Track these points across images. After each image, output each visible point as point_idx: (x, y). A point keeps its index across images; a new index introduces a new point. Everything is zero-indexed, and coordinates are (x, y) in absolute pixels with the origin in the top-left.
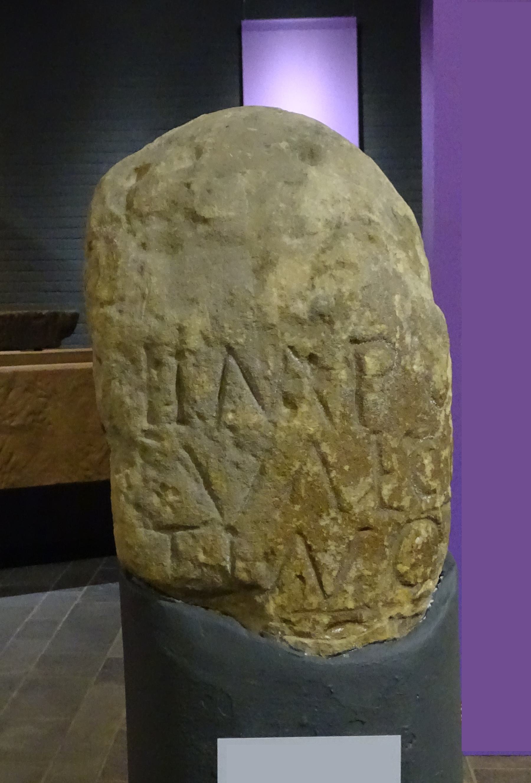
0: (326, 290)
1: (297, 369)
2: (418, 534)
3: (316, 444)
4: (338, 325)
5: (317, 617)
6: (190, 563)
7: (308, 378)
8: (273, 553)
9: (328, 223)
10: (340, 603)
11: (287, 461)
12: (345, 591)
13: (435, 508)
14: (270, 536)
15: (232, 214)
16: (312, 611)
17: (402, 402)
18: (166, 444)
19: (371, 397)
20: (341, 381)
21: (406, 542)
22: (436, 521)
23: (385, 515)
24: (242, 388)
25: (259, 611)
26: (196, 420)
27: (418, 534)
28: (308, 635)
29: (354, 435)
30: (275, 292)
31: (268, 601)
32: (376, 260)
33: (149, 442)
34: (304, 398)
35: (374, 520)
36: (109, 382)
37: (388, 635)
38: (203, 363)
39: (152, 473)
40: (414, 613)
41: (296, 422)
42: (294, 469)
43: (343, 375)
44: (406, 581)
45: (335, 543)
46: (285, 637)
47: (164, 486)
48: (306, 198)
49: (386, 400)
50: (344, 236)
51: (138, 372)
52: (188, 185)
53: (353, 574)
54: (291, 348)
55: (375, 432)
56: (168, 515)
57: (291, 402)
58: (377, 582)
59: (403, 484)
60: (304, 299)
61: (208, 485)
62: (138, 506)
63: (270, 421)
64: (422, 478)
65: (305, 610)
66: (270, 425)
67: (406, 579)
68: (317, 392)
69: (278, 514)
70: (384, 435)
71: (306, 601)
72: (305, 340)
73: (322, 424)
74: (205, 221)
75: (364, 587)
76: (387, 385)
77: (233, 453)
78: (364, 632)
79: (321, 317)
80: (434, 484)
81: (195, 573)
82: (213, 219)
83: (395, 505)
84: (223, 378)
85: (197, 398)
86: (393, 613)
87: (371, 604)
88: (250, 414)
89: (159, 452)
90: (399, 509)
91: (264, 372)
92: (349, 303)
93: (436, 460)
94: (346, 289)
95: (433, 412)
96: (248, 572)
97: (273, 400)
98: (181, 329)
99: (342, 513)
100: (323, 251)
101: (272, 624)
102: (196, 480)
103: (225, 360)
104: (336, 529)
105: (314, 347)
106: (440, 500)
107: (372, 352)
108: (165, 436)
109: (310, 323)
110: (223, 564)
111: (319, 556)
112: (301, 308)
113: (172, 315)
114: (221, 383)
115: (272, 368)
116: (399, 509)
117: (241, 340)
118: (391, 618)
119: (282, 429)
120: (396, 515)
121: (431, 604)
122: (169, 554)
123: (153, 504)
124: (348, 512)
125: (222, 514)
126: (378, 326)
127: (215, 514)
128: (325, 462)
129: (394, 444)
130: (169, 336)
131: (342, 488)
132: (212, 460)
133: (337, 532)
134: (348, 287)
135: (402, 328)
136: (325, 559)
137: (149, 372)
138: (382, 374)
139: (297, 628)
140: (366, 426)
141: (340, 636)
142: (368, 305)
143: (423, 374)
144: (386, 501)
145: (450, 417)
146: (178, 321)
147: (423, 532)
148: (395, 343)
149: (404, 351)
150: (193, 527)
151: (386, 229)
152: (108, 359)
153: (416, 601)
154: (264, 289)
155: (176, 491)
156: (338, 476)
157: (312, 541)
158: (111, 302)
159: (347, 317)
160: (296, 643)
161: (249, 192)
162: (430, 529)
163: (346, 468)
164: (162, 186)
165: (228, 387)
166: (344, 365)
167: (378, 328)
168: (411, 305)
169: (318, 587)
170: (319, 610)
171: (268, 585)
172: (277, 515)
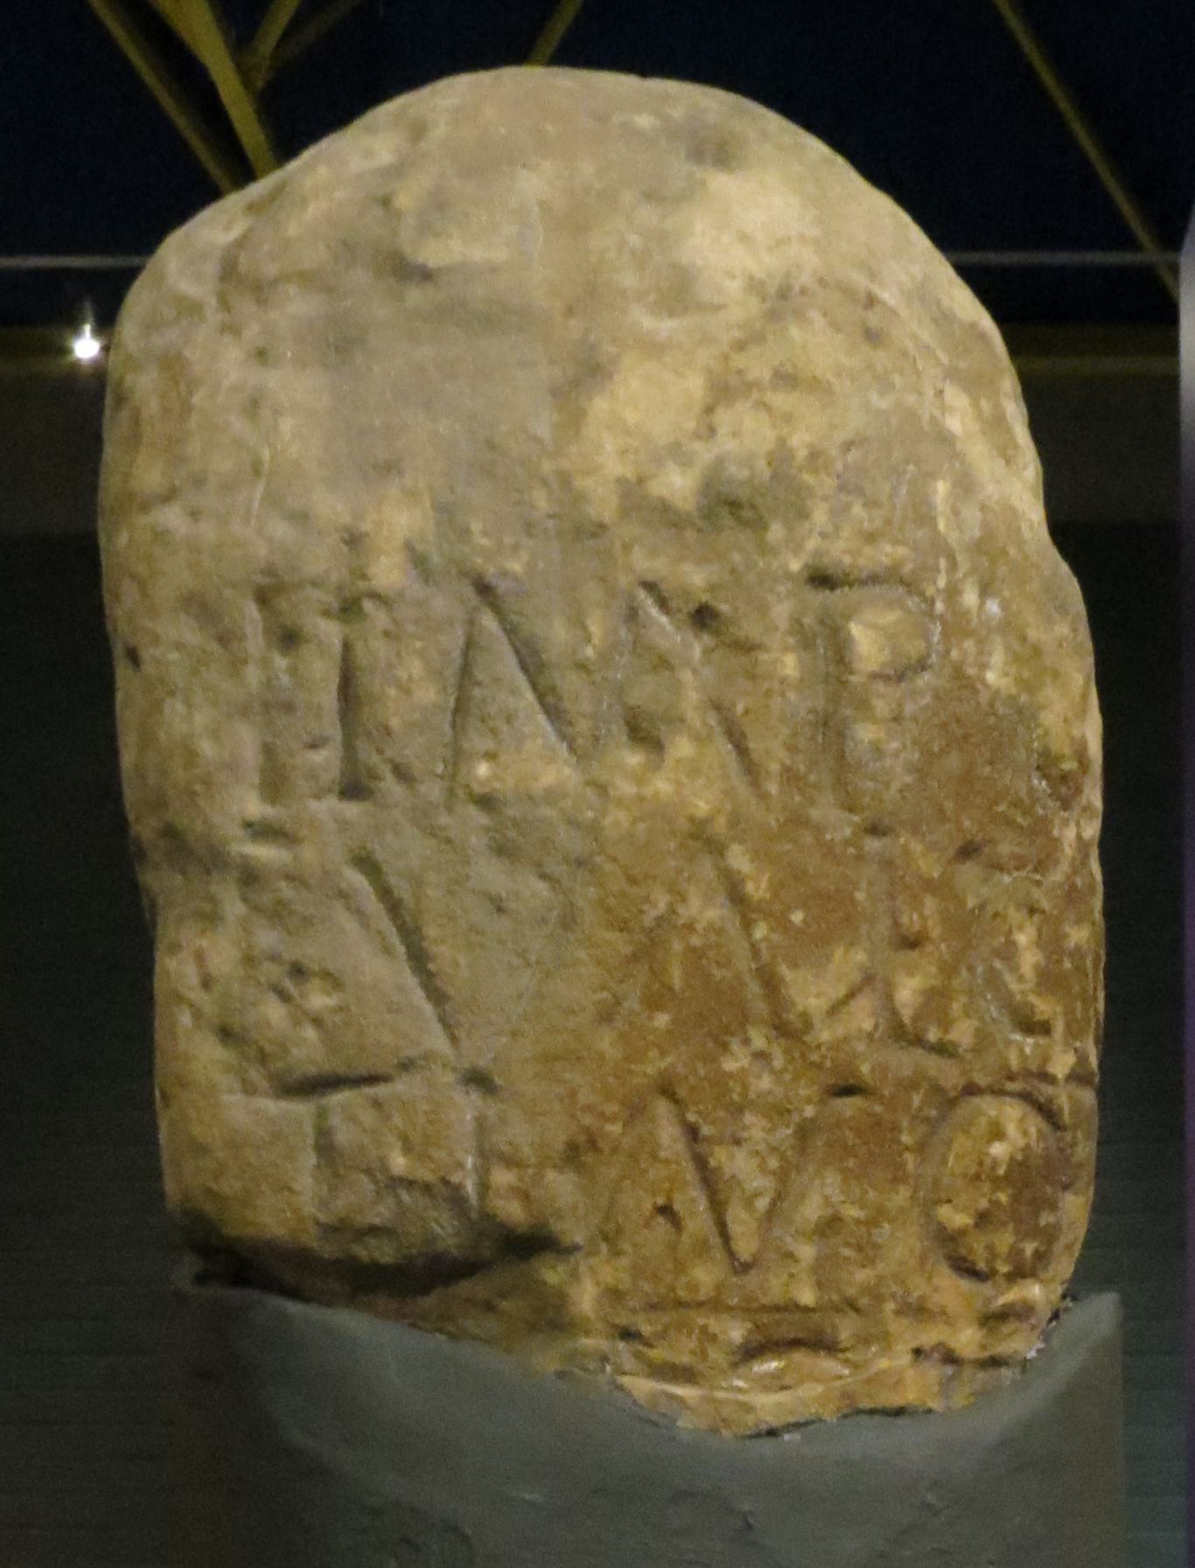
0: (746, 437)
1: (663, 644)
2: (997, 1133)
3: (716, 848)
4: (776, 532)
5: (713, 1324)
6: (364, 1179)
7: (694, 671)
8: (593, 1144)
9: (754, 286)
10: (774, 1286)
11: (634, 891)
12: (789, 1256)
13: (1049, 1079)
14: (584, 1097)
15: (500, 255)
16: (700, 1305)
17: (954, 762)
18: (308, 853)
19: (865, 733)
20: (783, 681)
21: (961, 1143)
22: (1047, 1112)
23: (905, 1061)
24: (514, 692)
25: (552, 1318)
26: (389, 785)
27: (997, 1133)
28: (686, 1375)
29: (818, 830)
30: (610, 444)
31: (575, 1276)
32: (886, 387)
33: (265, 853)
34: (683, 721)
35: (873, 1070)
36: (156, 707)
37: (909, 1396)
38: (411, 628)
39: (267, 938)
40: (986, 1354)
41: (662, 785)
42: (654, 913)
43: (790, 665)
44: (964, 1260)
45: (764, 1122)
46: (626, 1381)
47: (298, 971)
48: (698, 226)
49: (909, 744)
50: (799, 315)
51: (236, 665)
52: (386, 202)
53: (811, 1211)
54: (650, 587)
55: (875, 830)
56: (308, 1051)
57: (644, 733)
58: (880, 1241)
59: (956, 982)
60: (685, 461)
61: (419, 959)
62: (226, 1034)
63: (588, 783)
64: (1008, 978)
65: (680, 1304)
66: (590, 792)
67: (963, 1252)
68: (717, 707)
69: (607, 1040)
70: (902, 840)
71: (683, 1280)
72: (687, 567)
73: (729, 793)
74: (426, 275)
75: (847, 1252)
76: (909, 708)
77: (492, 874)
78: (840, 1377)
79: (730, 507)
80: (1044, 1007)
81: (381, 1208)
82: (449, 270)
83: (932, 1035)
84: (466, 671)
85: (395, 722)
86: (929, 1336)
87: (864, 1302)
88: (535, 763)
89: (290, 878)
90: (943, 1049)
91: (574, 652)
92: (808, 478)
93: (1051, 942)
94: (799, 441)
95: (1041, 812)
96: (525, 1197)
97: (598, 728)
98: (354, 541)
99: (783, 1041)
100: (740, 346)
101: (587, 1342)
102: (387, 950)
103: (471, 622)
104: (765, 1083)
105: (712, 588)
106: (1062, 1064)
107: (869, 615)
108: (304, 832)
109: (699, 523)
110: (455, 1178)
111: (722, 1158)
112: (678, 485)
113: (330, 507)
114: (461, 688)
115: (596, 640)
116: (943, 1049)
117: (516, 566)
118: (918, 1352)
119: (620, 802)
120: (933, 1065)
121: (1038, 1351)
122: (310, 1159)
123: (269, 1024)
124: (799, 1039)
125: (454, 1040)
126: (888, 548)
127: (437, 1041)
128: (737, 898)
129: (930, 867)
130: (321, 559)
131: (785, 971)
132: (430, 892)
133: (770, 1092)
134: (807, 438)
135: (953, 565)
136: (737, 1164)
137: (265, 663)
138: (900, 673)
139: (656, 1354)
140: (851, 810)
141: (777, 1383)
142: (860, 491)
143: (1010, 696)
144: (907, 1020)
145: (1094, 853)
146: (346, 519)
147: (1012, 1130)
148: (932, 602)
149: (958, 625)
150: (372, 1079)
151: (915, 329)
152: (156, 640)
153: (994, 1320)
154: (577, 433)
155: (333, 980)
156: (775, 937)
157: (699, 1113)
158: (169, 496)
159: (804, 514)
160: (654, 1396)
161: (544, 206)
162: (1033, 1130)
163: (797, 917)
164: (314, 210)
165: (477, 692)
166: (791, 641)
167: (886, 553)
168: (979, 515)
169: (715, 1240)
170: (715, 1305)
171: (574, 1232)
172: (606, 1042)
